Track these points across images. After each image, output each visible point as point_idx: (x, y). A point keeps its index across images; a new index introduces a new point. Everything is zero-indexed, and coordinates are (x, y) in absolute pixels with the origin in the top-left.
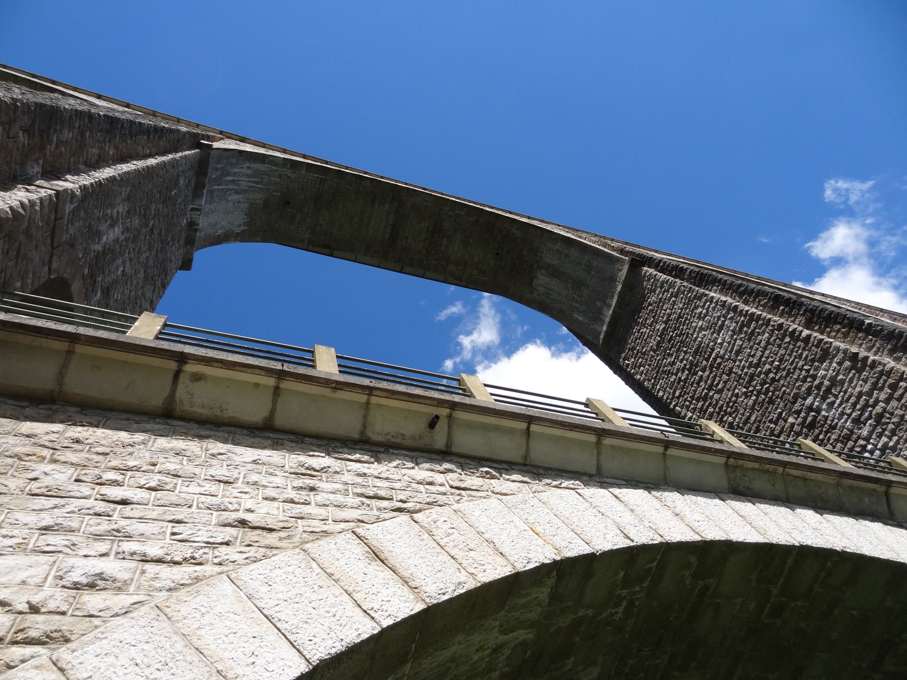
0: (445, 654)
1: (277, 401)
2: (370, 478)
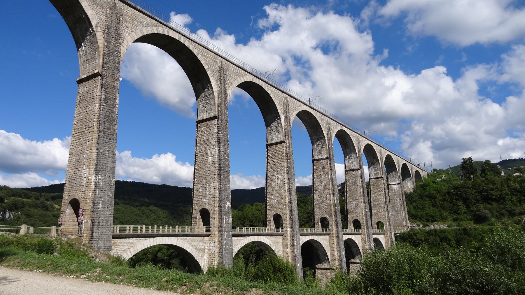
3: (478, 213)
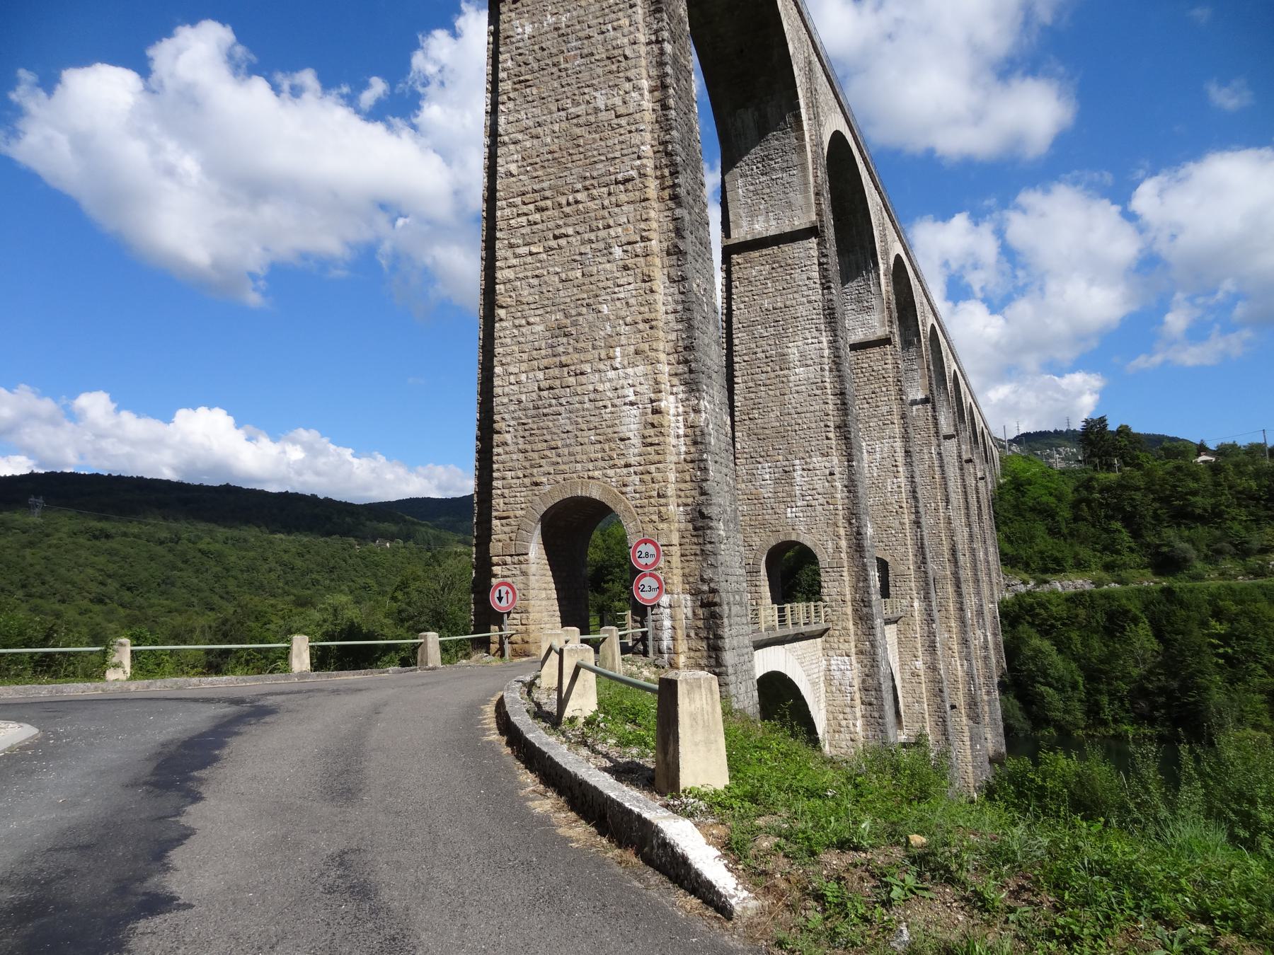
3: (1165, 549)
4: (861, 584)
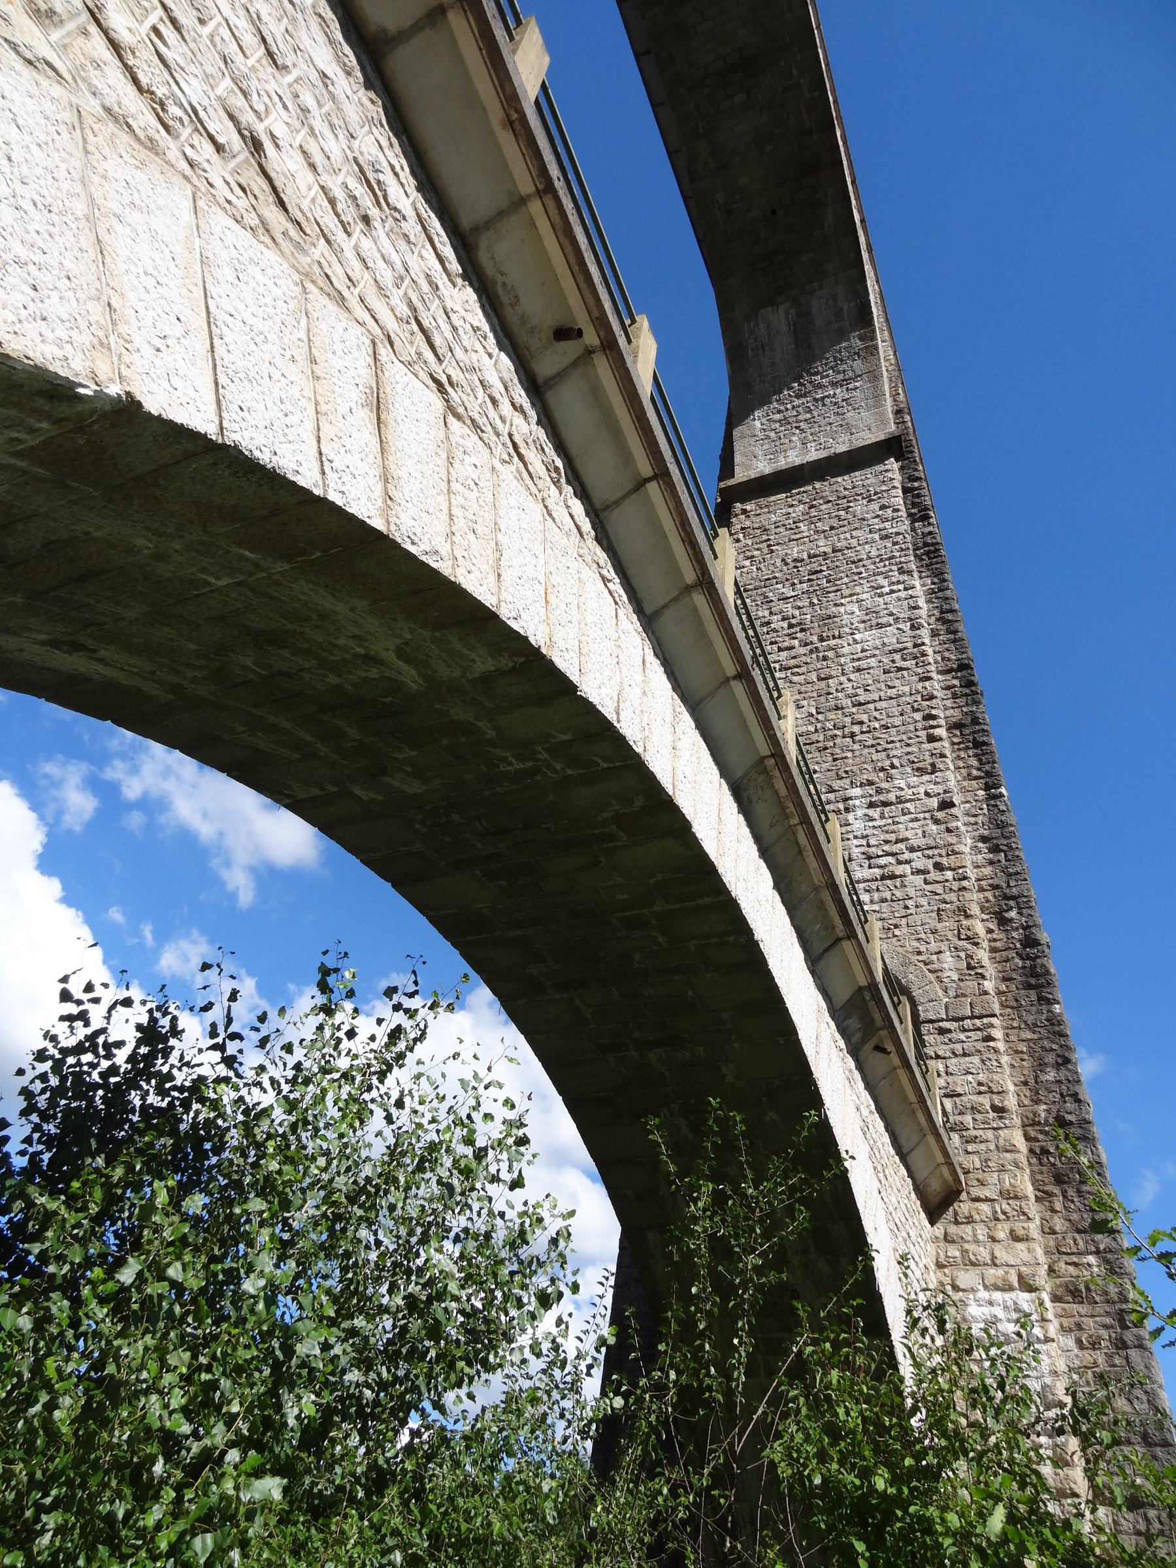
0: (325, 601)
1: (422, 29)
2: (437, 301)
4: (1051, 1075)
